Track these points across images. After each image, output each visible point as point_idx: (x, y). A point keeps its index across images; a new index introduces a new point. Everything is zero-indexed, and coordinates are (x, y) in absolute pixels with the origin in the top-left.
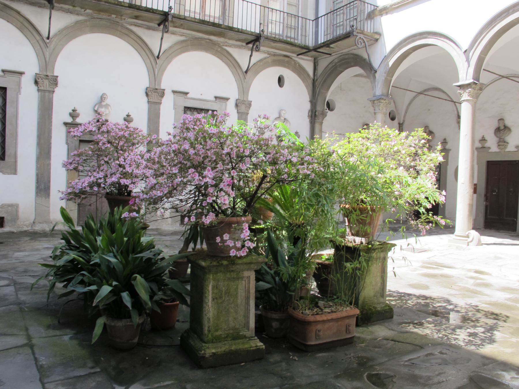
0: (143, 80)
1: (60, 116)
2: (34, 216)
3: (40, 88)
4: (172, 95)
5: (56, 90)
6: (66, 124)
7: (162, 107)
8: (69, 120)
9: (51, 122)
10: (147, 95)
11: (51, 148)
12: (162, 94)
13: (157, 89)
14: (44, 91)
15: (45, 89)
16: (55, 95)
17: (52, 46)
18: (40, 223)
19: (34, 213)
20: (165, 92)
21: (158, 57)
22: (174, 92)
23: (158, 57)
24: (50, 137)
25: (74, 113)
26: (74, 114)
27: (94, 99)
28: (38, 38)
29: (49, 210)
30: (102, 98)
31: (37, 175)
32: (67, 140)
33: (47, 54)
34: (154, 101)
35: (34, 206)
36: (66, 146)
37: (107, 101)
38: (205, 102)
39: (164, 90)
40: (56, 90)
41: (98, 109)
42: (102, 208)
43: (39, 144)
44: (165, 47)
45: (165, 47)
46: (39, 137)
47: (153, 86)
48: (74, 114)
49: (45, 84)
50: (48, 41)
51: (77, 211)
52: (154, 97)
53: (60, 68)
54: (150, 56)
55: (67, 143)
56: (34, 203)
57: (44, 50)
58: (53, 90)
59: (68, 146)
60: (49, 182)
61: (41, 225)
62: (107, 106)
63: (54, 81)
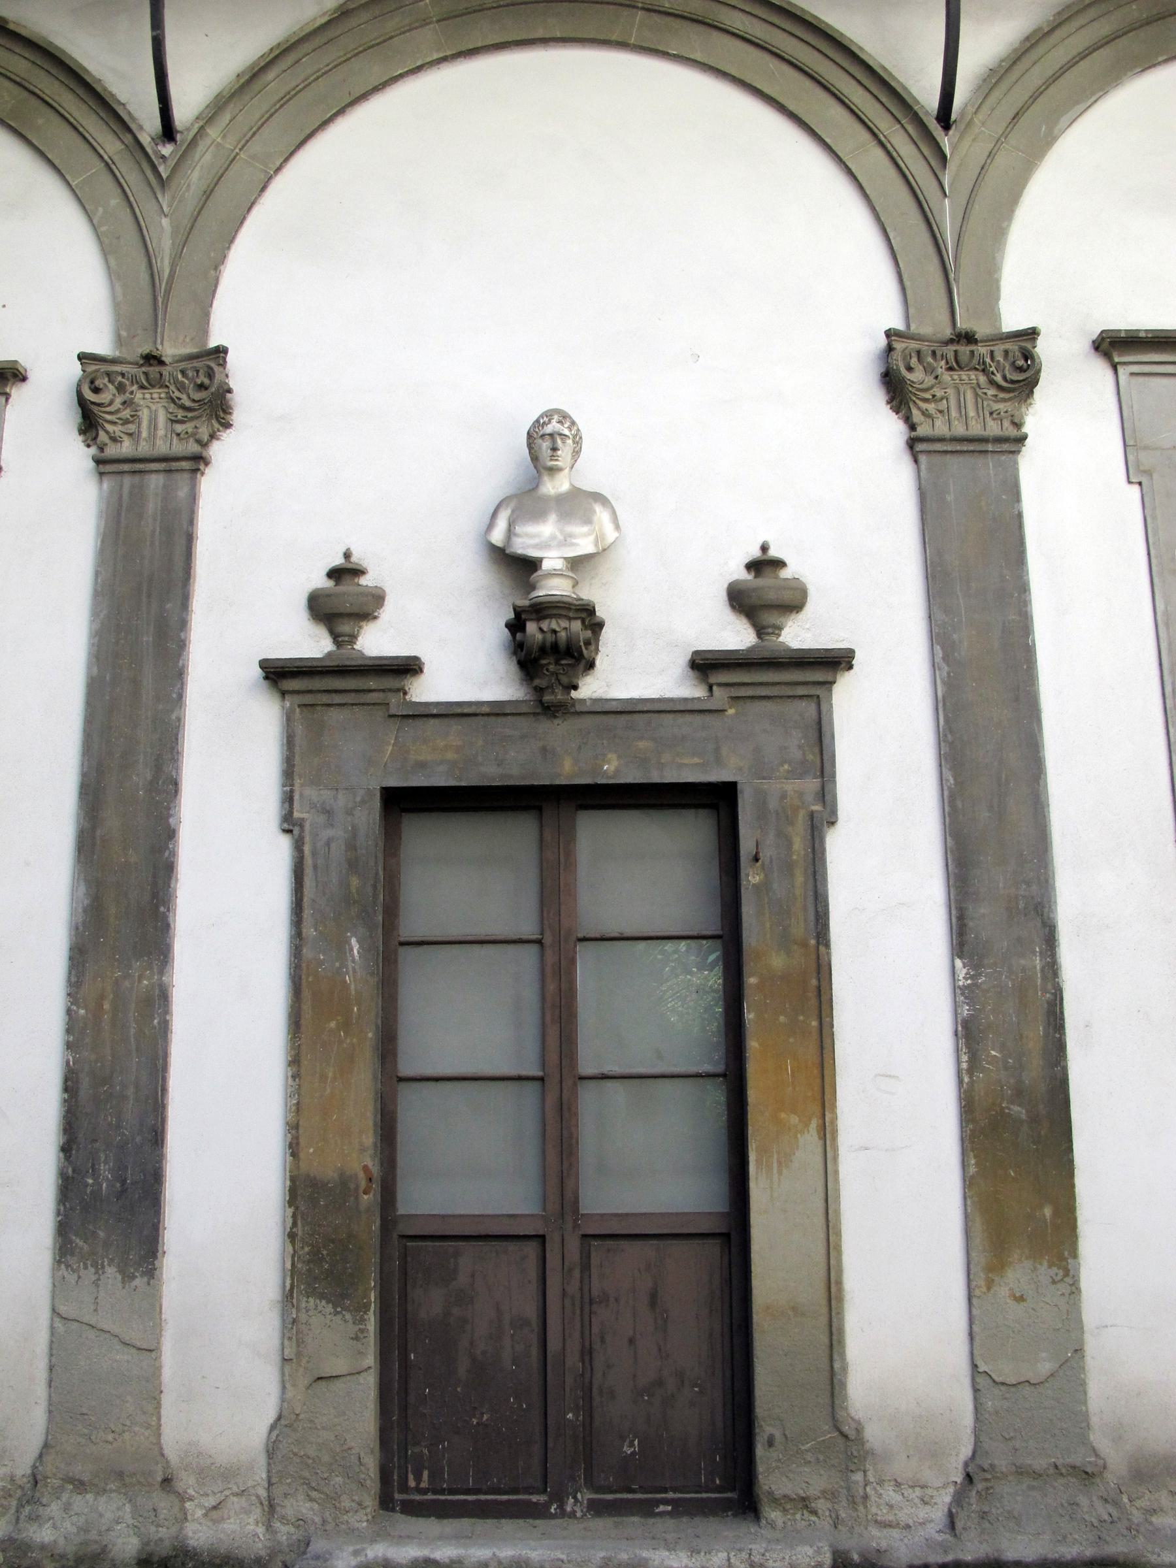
0: (856, 291)
1: (244, 612)
2: (39, 1416)
3: (112, 451)
4: (1100, 371)
5: (226, 452)
6: (278, 674)
7: (1031, 467)
8: (310, 643)
9: (180, 675)
10: (896, 388)
11: (169, 868)
12: (1016, 368)
13: (968, 338)
14: (137, 464)
15: (144, 449)
16: (210, 485)
17: (195, 177)
18: (80, 1486)
19: (40, 1391)
20: (1043, 348)
21: (944, 116)
22: (1113, 346)
23: (944, 116)
24: (165, 788)
25: (346, 588)
26: (342, 600)
27: (497, 462)
28: (111, 145)
29: (157, 1371)
30: (545, 442)
31: (70, 1084)
32: (288, 799)
33: (947, 217)
34: (959, 430)
35: (42, 1339)
36: (283, 846)
37: (590, 469)
38: (302, 138)
39: (1032, 334)
40: (216, 450)
41: (510, 533)
42: (587, 1353)
43: (90, 846)
44: (981, 48)
45: (981, 48)
46: (93, 794)
47: (936, 325)
48: (342, 600)
49: (153, 423)
50: (167, 150)
51: (370, 1381)
52: (960, 408)
53: (255, 309)
54: (883, 123)
55: (289, 824)
56: (44, 1315)
57: (146, 207)
58: (192, 448)
59: (298, 846)
60: (157, 1137)
61: (81, 1503)
62: (579, 504)
63: (206, 395)
